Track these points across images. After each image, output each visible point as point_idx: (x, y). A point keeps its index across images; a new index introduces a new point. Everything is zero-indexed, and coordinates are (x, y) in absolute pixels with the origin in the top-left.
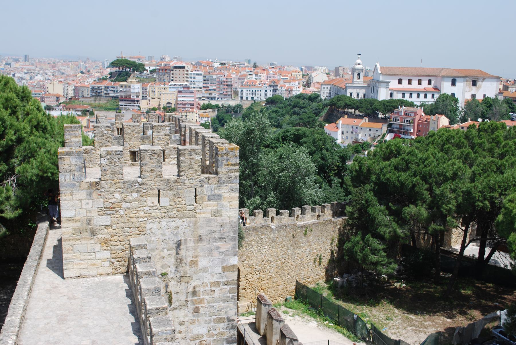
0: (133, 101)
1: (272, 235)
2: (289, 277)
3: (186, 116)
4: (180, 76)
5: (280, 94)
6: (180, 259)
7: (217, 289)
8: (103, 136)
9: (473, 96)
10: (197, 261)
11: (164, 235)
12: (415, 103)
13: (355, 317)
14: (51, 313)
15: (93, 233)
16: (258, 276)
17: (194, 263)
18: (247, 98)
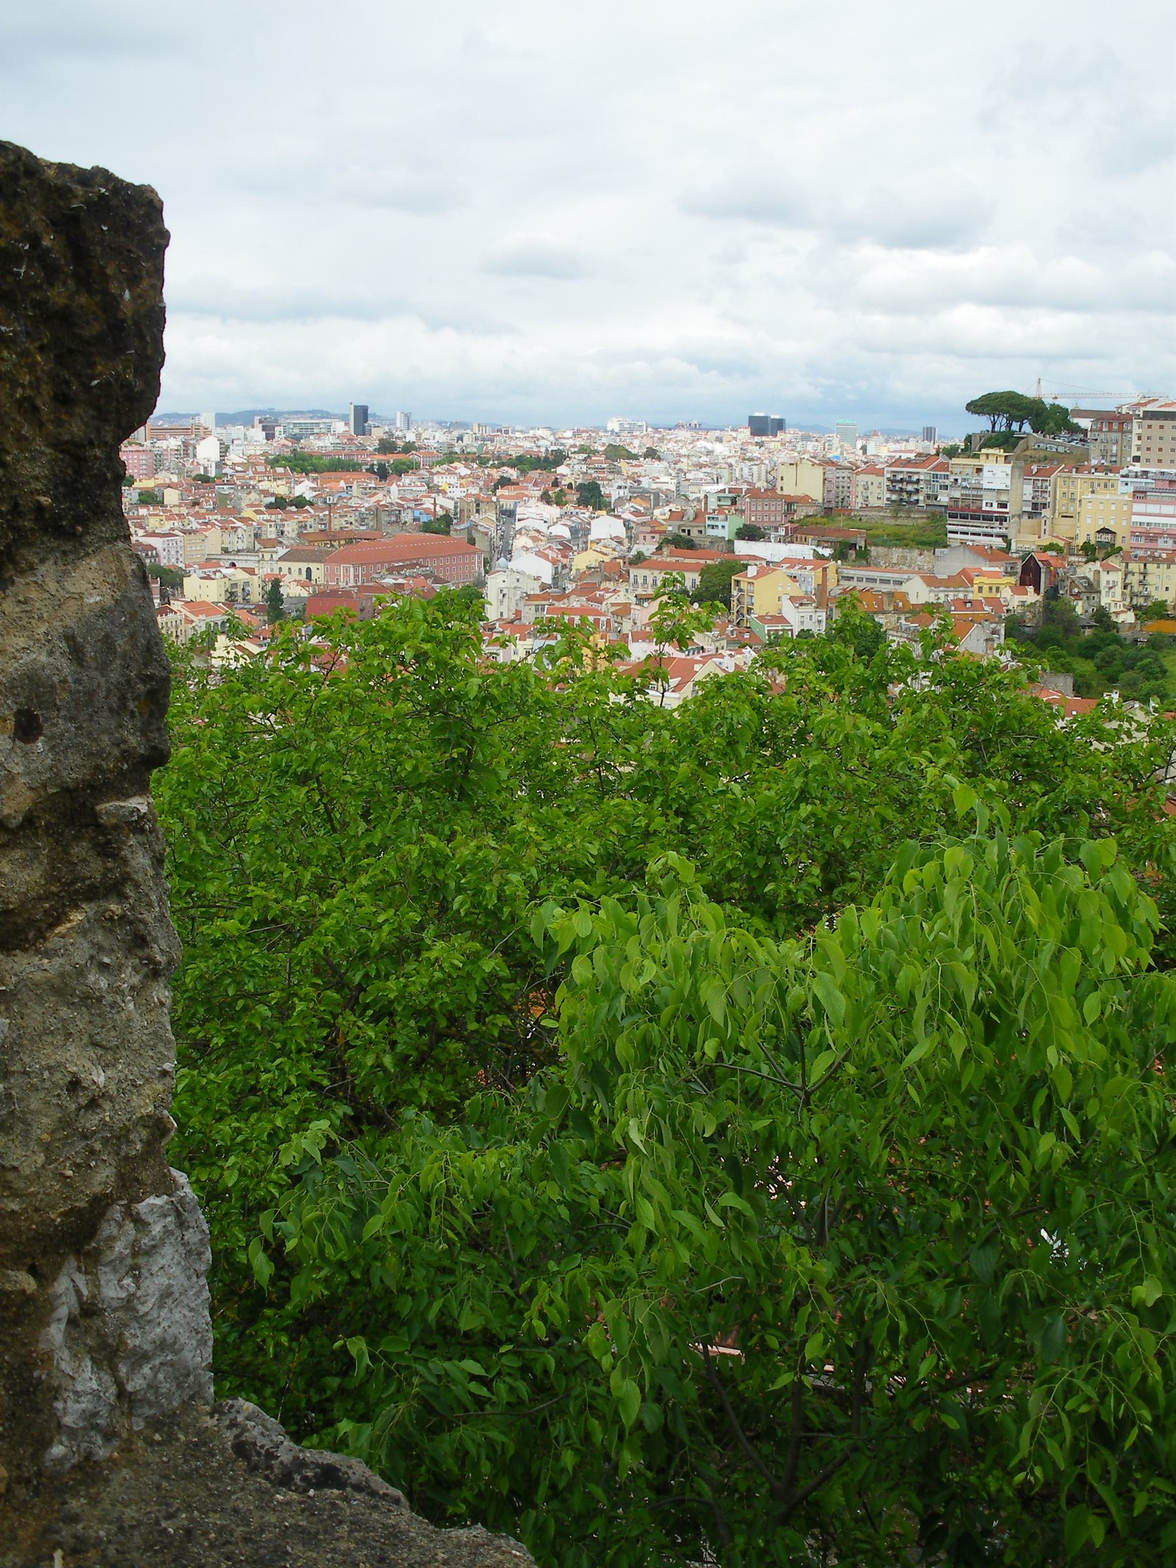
0: (988, 517)
3: (1145, 574)
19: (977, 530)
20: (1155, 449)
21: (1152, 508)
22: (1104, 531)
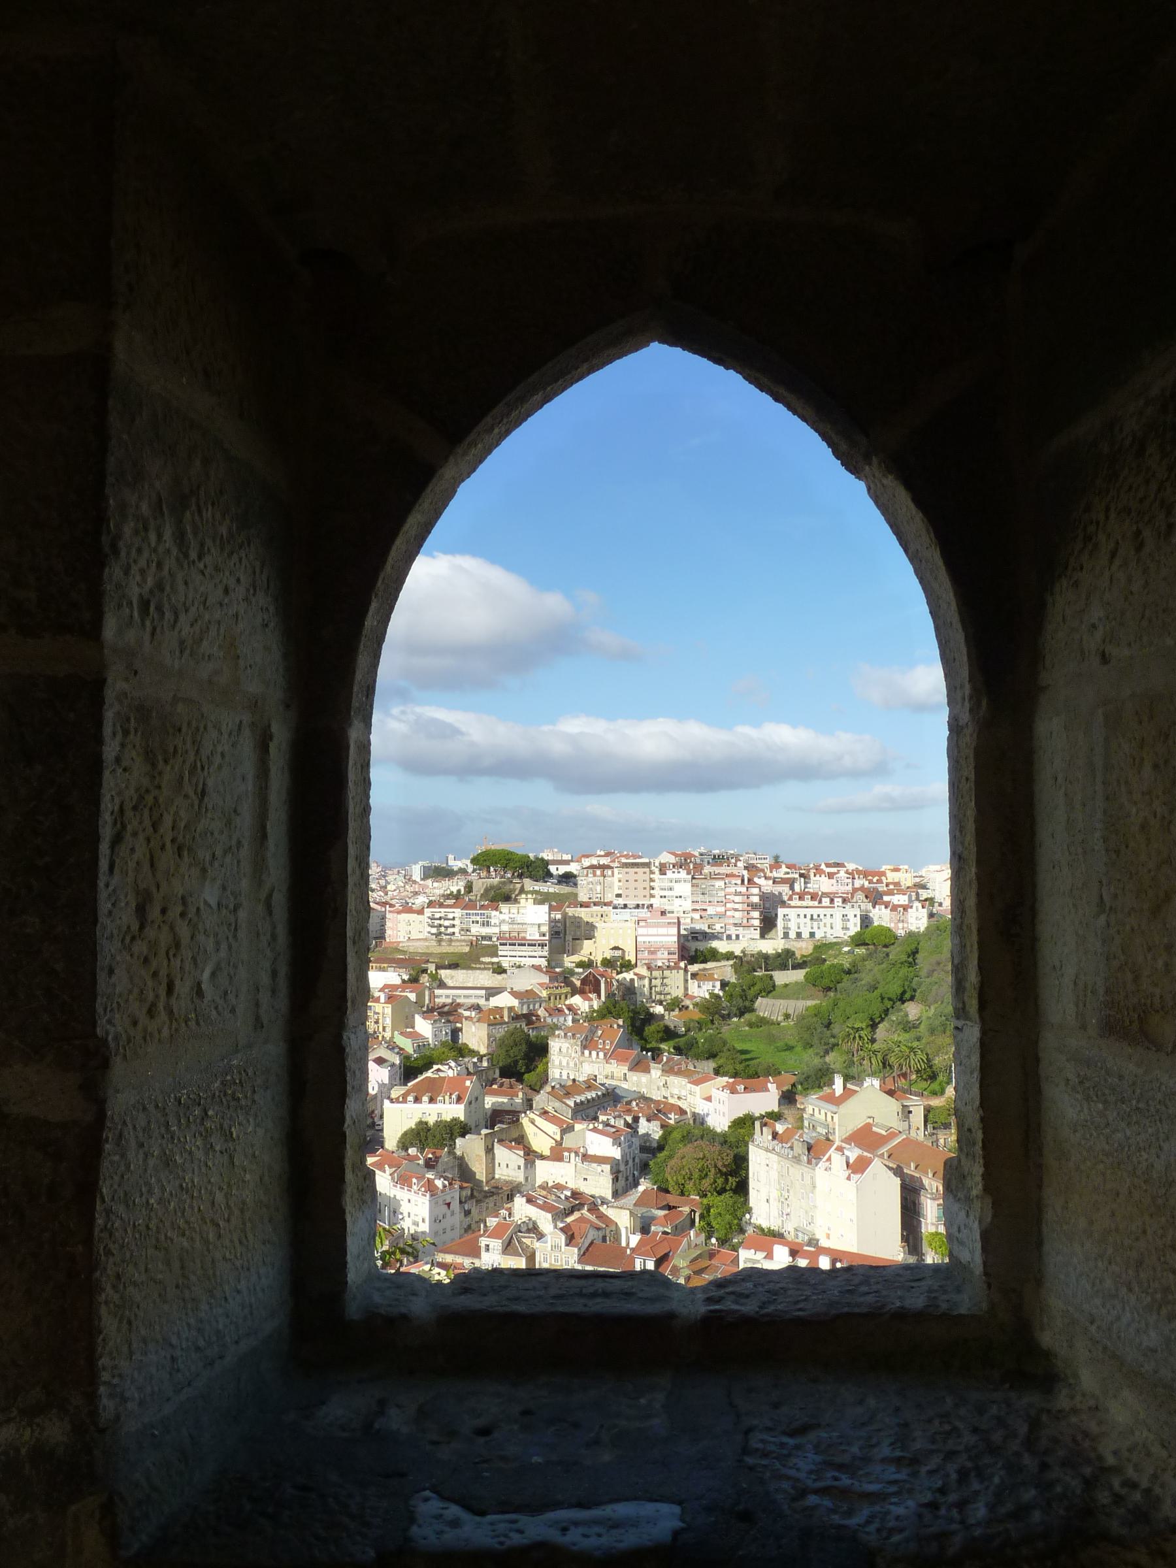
18: (799, 935)
22: (616, 948)
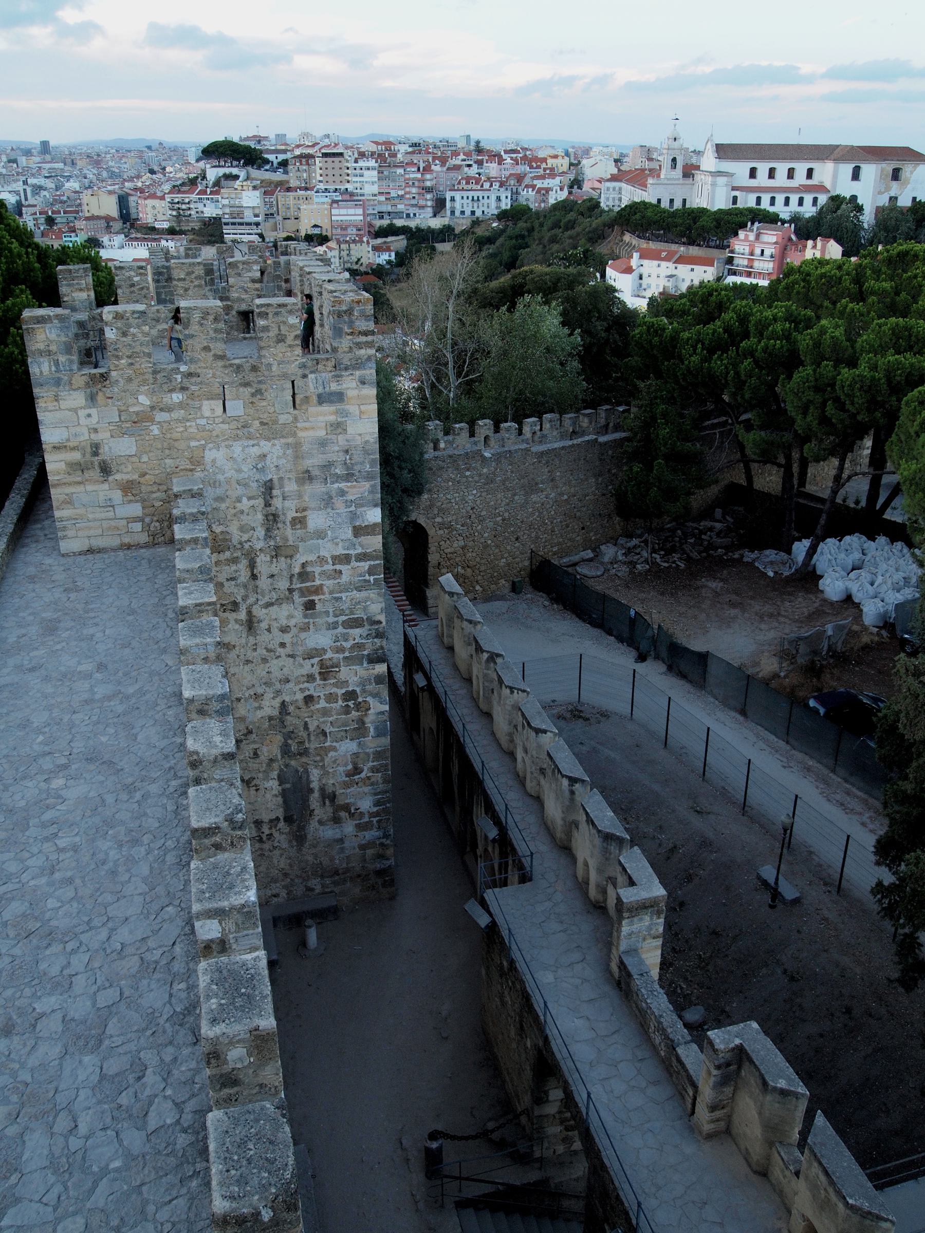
1: (485, 470)
2: (517, 544)
3: (349, 250)
4: (334, 172)
5: (525, 203)
6: (274, 515)
7: (344, 568)
8: (133, 285)
9: (893, 199)
10: (305, 517)
11: (239, 471)
12: (782, 216)
13: (632, 613)
14: (32, 618)
15: (105, 470)
16: (462, 543)
17: (300, 522)
18: (463, 213)
19: (243, 231)
20: (337, 175)
21: (343, 211)
22: (315, 226)
